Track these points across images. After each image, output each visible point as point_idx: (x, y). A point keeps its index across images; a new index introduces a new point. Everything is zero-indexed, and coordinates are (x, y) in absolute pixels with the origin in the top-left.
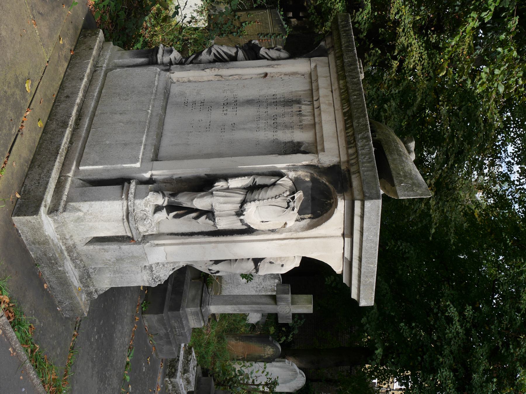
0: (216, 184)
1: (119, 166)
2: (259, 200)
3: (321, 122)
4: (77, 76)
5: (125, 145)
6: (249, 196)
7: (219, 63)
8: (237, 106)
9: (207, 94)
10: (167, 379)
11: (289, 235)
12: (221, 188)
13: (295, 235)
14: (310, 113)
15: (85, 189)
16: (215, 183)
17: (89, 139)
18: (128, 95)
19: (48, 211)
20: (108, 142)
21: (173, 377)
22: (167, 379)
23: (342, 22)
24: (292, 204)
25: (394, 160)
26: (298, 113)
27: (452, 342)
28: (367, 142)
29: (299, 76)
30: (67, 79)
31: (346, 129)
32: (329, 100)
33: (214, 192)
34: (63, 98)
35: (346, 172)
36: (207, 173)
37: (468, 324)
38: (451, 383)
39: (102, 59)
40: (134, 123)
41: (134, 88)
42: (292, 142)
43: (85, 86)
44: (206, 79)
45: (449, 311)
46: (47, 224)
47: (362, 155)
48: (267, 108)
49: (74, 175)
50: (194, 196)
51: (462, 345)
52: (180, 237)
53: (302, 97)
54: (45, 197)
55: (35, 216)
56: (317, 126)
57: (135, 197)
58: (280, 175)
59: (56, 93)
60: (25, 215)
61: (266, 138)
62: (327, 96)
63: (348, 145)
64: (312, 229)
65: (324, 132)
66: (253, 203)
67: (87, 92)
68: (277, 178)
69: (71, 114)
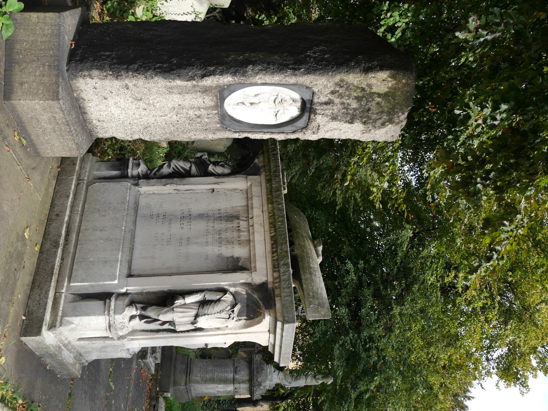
1: (101, 283)
2: (208, 315)
3: (254, 241)
5: (105, 262)
7: (177, 179)
9: (169, 207)
11: (230, 331)
13: (234, 332)
18: (105, 211)
20: (92, 259)
21: (144, 359)
24: (232, 316)
25: (306, 279)
28: (287, 268)
29: (238, 191)
31: (273, 253)
32: (260, 221)
33: (175, 309)
34: (54, 217)
36: (170, 289)
39: (83, 171)
40: (111, 240)
41: (110, 203)
42: (232, 257)
43: (71, 202)
44: (166, 192)
46: (48, 338)
47: (284, 280)
48: (214, 223)
49: (66, 291)
56: (251, 243)
58: (224, 291)
60: (30, 336)
62: (259, 216)
66: (203, 317)
67: (72, 207)
69: (61, 234)
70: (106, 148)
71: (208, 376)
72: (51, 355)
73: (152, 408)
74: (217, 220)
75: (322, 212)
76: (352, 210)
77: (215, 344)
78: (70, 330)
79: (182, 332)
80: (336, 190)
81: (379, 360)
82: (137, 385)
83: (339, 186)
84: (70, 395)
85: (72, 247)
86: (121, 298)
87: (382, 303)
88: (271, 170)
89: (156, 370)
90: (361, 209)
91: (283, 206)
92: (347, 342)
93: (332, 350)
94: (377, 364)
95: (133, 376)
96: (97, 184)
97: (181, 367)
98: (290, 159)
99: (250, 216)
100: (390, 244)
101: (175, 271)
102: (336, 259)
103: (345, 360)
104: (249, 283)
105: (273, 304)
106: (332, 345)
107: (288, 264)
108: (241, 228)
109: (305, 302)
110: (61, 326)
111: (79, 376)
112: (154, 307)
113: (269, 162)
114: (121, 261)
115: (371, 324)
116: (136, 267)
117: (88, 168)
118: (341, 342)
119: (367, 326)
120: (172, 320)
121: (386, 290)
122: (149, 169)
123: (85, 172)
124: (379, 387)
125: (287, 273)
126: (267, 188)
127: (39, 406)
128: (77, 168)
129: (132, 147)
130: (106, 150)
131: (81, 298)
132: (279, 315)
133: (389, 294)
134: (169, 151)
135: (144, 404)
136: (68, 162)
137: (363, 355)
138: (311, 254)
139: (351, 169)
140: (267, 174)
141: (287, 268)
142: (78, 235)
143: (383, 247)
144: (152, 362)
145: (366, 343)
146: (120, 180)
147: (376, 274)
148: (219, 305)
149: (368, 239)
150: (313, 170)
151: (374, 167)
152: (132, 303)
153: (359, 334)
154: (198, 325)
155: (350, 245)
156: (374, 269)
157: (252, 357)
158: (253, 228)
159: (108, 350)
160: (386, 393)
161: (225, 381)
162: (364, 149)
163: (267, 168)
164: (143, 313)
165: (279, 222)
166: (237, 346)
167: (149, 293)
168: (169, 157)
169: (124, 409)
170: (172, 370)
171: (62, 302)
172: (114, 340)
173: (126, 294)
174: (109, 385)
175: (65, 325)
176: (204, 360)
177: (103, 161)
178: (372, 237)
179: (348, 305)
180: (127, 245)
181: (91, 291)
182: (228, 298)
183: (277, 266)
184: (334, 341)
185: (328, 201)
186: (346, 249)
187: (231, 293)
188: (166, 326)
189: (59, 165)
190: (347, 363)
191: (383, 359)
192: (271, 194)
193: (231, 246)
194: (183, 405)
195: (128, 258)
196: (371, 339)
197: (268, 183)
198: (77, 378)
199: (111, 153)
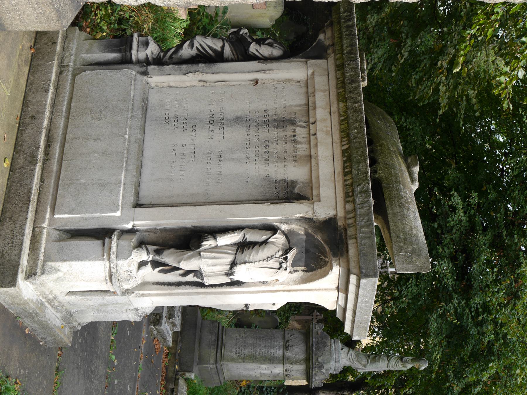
0: (204, 243)
1: (98, 215)
2: (250, 263)
3: (317, 157)
4: (42, 86)
5: (103, 185)
6: (239, 257)
8: (224, 126)
10: (152, 327)
12: (209, 247)
14: (305, 139)
15: (64, 243)
16: (203, 242)
17: (61, 175)
18: (101, 111)
19: (26, 275)
20: (83, 181)
21: (158, 324)
22: (152, 327)
23: (345, 12)
24: (284, 265)
25: (395, 214)
26: (292, 138)
27: (454, 230)
28: (366, 197)
29: (294, 83)
30: (30, 90)
31: (345, 174)
33: (202, 253)
34: (28, 120)
35: (343, 231)
36: (194, 224)
37: (473, 211)
38: (450, 272)
39: (67, 54)
40: (110, 154)
41: (107, 101)
42: (285, 181)
43: (52, 99)
44: (188, 84)
45: (453, 200)
46: (26, 290)
47: (361, 215)
48: (258, 129)
49: (49, 225)
50: (181, 257)
51: (464, 232)
52: (166, 286)
53: (296, 116)
54: (21, 261)
55: (12, 288)
56: (313, 160)
57: (117, 257)
58: (273, 229)
59: (19, 114)
61: (257, 174)
62: (325, 120)
63: (346, 198)
64: (305, 283)
65: (320, 174)
66: (243, 265)
67: (54, 105)
68: (269, 233)
69: (39, 144)
70: (99, 21)
71: (247, 352)
72: (30, 314)
73: (169, 393)
74: (262, 126)
75: (417, 119)
76: (462, 117)
77: (259, 305)
78: (56, 281)
79: (212, 286)
80: (439, 84)
81: (497, 339)
82: (148, 361)
83: (444, 78)
84: (57, 369)
85: (56, 164)
86: (125, 236)
87: (504, 256)
88: (343, 50)
89: (175, 341)
90: (477, 114)
91: (361, 105)
92: (449, 311)
93: (427, 321)
94: (493, 345)
95: (142, 348)
96: (88, 72)
97: (208, 337)
98: (369, 39)
99: (312, 120)
100: (520, 168)
101: (202, 199)
102: (436, 189)
103: (446, 337)
104: (309, 219)
105: (344, 249)
106: (426, 314)
107: (367, 191)
108: (298, 138)
109: (392, 248)
110: (43, 273)
111: (70, 345)
112: (172, 250)
113: (341, 38)
114: (124, 184)
115: (487, 286)
116: (146, 195)
117: (74, 49)
118: (440, 311)
119: (481, 289)
120: (198, 269)
121: (512, 236)
122: (162, 51)
123: (71, 54)
124: (495, 378)
125: (366, 205)
126: (337, 79)
127: (16, 383)
128: (58, 48)
129: (136, 19)
130: (98, 24)
131: (70, 235)
132: (353, 265)
133: (516, 244)
134: (190, 25)
135: (158, 386)
136: (45, 40)
137: (474, 331)
138: (402, 177)
139: (466, 47)
140: (338, 56)
141: (366, 197)
142: (63, 147)
143: (508, 173)
144: (168, 329)
145: (478, 314)
146: (120, 66)
147: (496, 213)
148: (266, 249)
149: (485, 161)
150: (406, 55)
151: (500, 49)
152: (141, 244)
153: (468, 300)
154: (236, 277)
155: (459, 169)
156: (494, 205)
157: (313, 324)
158: (316, 139)
159: (109, 308)
160: (506, 387)
161: (271, 360)
162: (488, 15)
163: (337, 48)
164: (157, 258)
165: (355, 128)
166: (291, 309)
167: (164, 230)
168: (189, 34)
169: (130, 392)
170: (197, 341)
171: (44, 241)
172: (117, 295)
173: (132, 231)
174: (111, 359)
175: (49, 273)
176: (241, 329)
177: (94, 39)
178: (492, 157)
179: (453, 258)
180: (133, 161)
181: (84, 226)
182: (279, 239)
183: (351, 194)
184: (430, 309)
185: (426, 103)
186: (452, 174)
187: (283, 232)
188: (190, 278)
189: (32, 44)
190: (448, 342)
191: (503, 339)
192: (343, 87)
193: (284, 164)
194: (212, 391)
195: (135, 180)
196: (486, 308)
197: (339, 70)
198: (66, 347)
199: (105, 28)
